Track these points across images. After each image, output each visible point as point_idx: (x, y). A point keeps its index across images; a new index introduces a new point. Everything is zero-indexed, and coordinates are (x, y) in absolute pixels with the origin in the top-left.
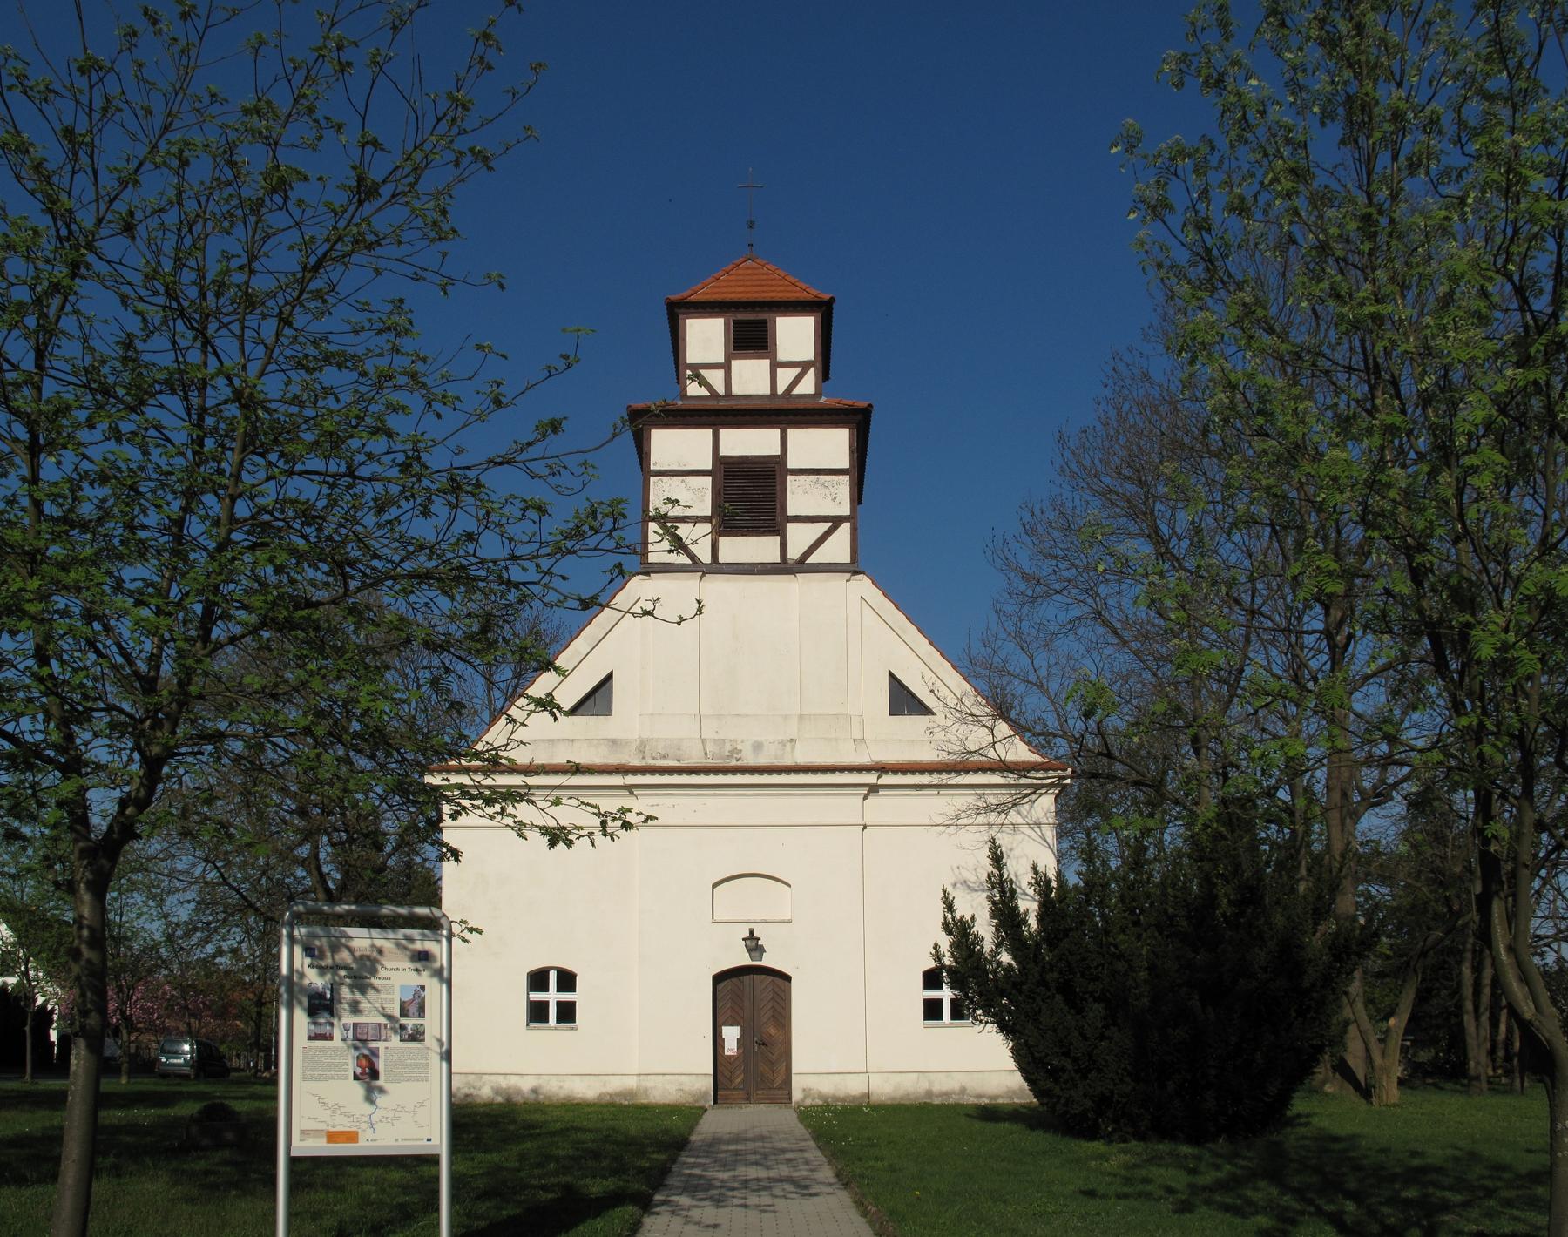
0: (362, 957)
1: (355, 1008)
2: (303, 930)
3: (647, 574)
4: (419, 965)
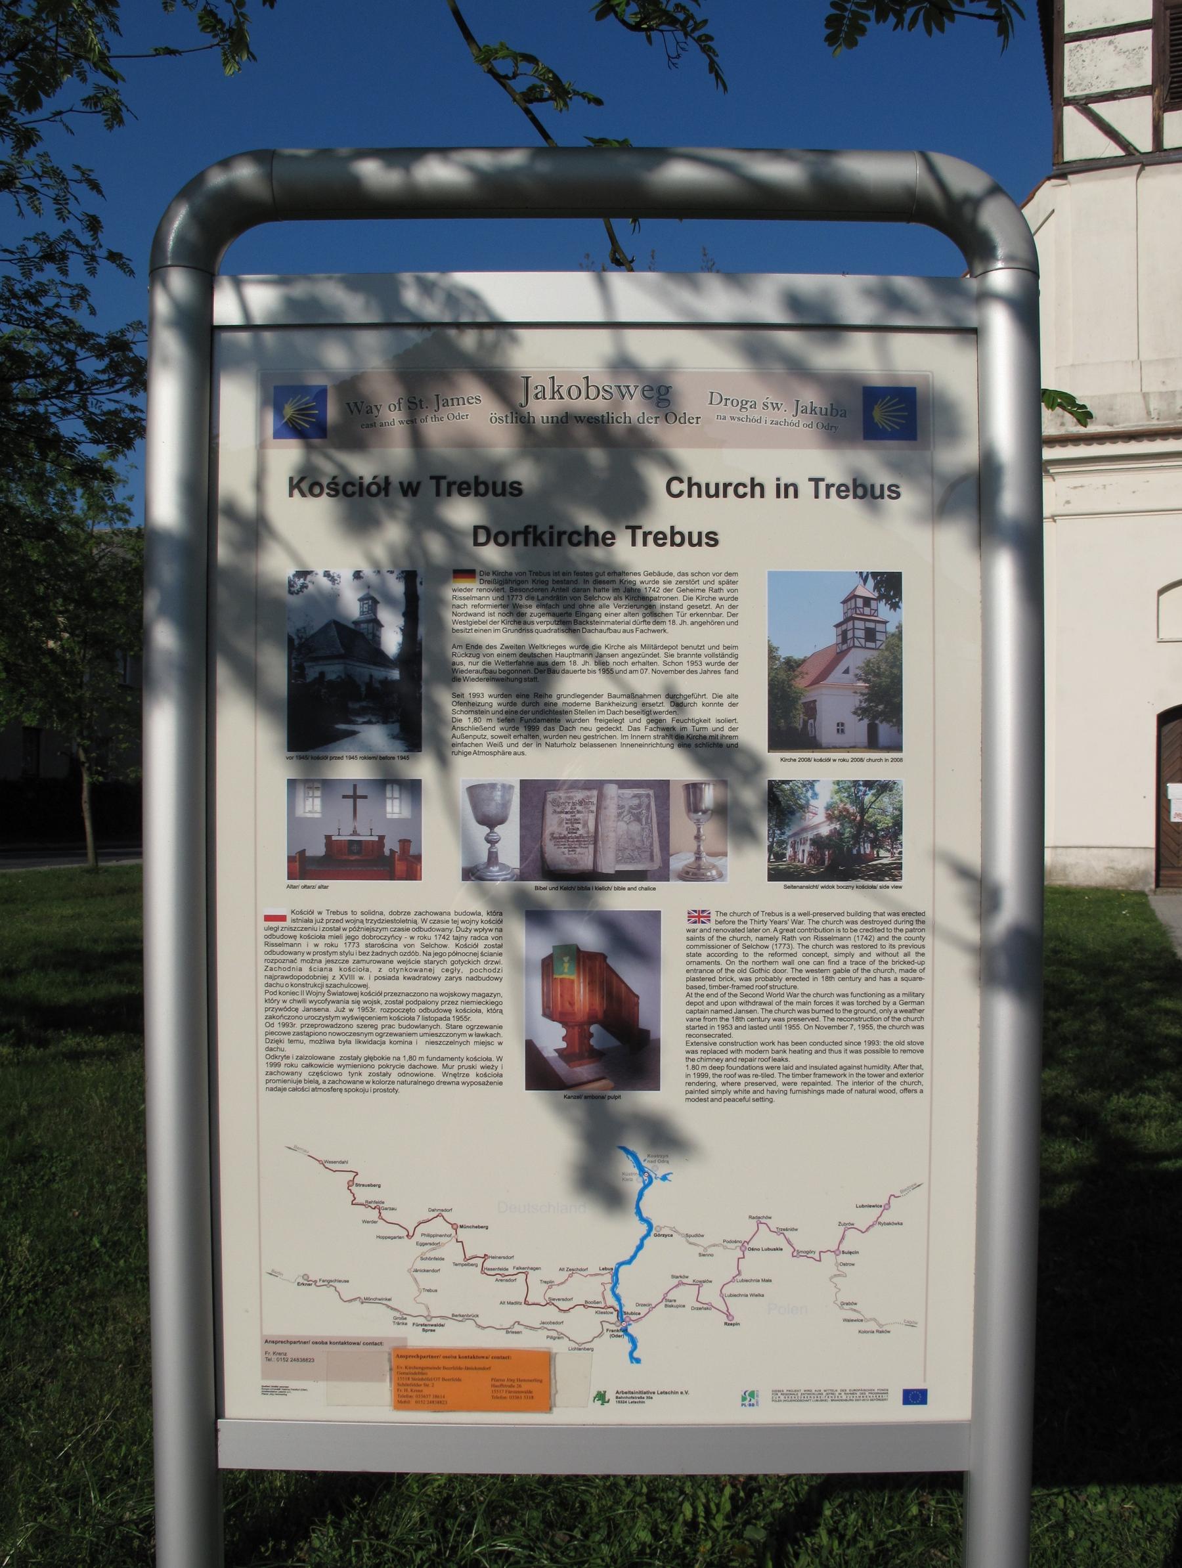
0: (564, 421)
1: (530, 698)
2: (262, 298)
3: (1063, 176)
4: (870, 462)
